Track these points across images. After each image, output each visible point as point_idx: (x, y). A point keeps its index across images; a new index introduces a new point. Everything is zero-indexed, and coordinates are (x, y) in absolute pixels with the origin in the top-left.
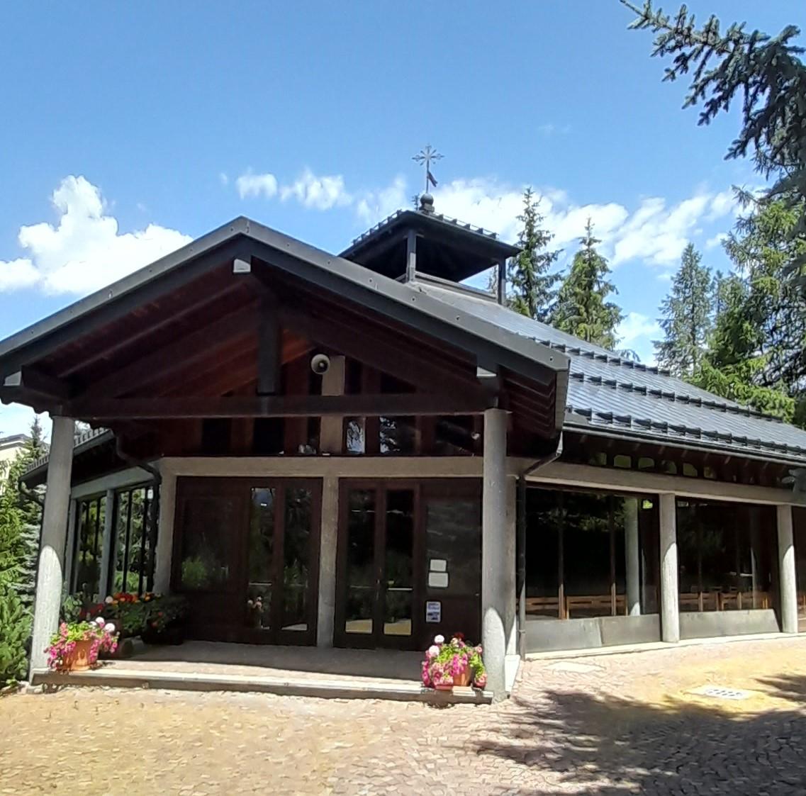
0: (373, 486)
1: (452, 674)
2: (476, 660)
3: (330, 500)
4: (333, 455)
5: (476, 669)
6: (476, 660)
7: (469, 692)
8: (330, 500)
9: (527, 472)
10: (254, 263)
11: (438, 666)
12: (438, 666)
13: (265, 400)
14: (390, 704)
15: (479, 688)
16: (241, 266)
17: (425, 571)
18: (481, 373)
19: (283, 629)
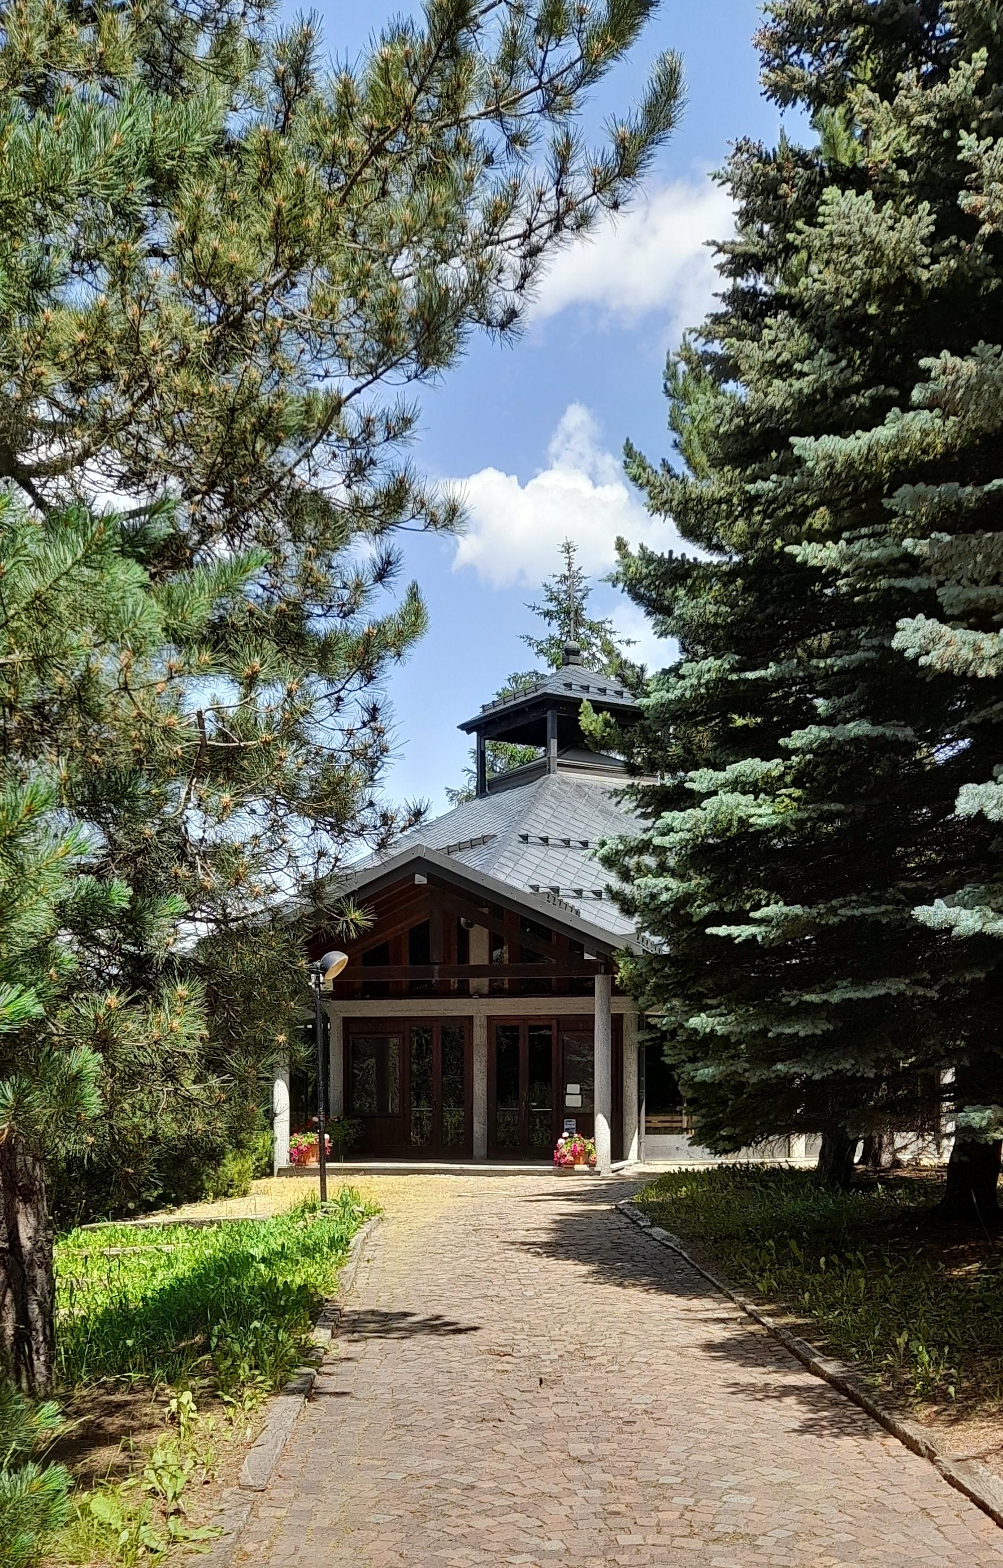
0: (514, 1023)
1: (573, 1155)
2: (590, 1147)
3: (480, 1035)
4: (481, 996)
5: (590, 1152)
6: (590, 1147)
7: (586, 1168)
8: (480, 1035)
9: (646, 1009)
10: (429, 877)
11: (564, 1150)
12: (564, 1150)
13: (436, 967)
14: (545, 1270)
15: (592, 1165)
16: (420, 879)
17: (562, 1094)
18: (587, 956)
19: (709, 931)
